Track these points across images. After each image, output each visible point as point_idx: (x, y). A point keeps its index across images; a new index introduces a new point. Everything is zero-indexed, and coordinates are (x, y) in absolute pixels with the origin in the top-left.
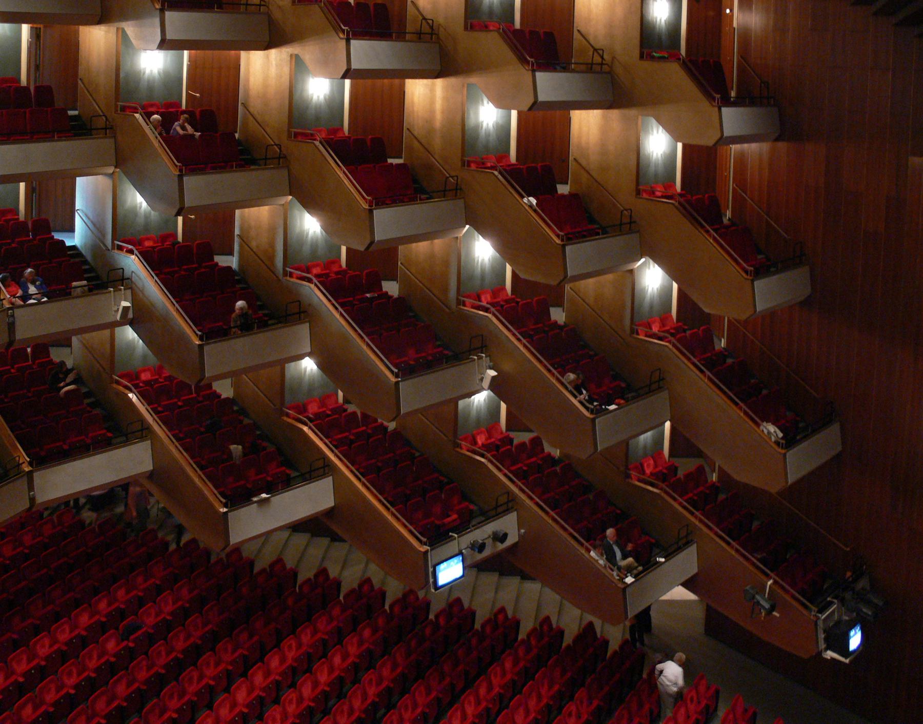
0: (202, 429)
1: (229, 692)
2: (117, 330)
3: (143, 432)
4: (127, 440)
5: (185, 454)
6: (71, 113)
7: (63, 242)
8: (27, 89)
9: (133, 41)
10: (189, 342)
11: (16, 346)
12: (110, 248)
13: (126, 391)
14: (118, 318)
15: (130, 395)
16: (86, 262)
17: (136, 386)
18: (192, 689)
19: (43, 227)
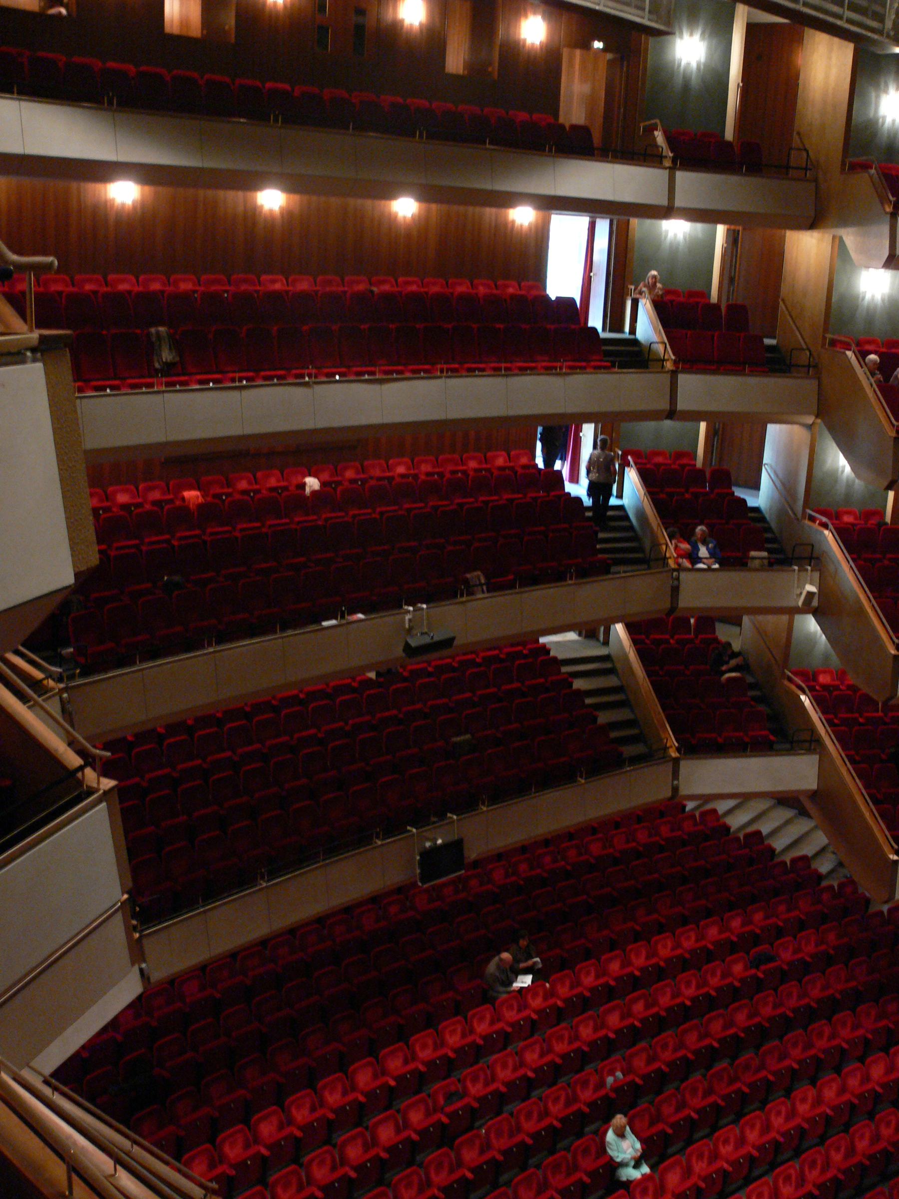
0: (884, 757)
1: (863, 1063)
2: (798, 618)
3: (813, 744)
4: (792, 749)
5: (858, 781)
6: (768, 341)
7: (744, 501)
8: (717, 307)
9: (853, 254)
10: (883, 648)
11: (677, 614)
12: (800, 515)
13: (799, 692)
14: (800, 604)
15: (803, 697)
16: (769, 529)
17: (812, 689)
18: (822, 1043)
19: (723, 479)
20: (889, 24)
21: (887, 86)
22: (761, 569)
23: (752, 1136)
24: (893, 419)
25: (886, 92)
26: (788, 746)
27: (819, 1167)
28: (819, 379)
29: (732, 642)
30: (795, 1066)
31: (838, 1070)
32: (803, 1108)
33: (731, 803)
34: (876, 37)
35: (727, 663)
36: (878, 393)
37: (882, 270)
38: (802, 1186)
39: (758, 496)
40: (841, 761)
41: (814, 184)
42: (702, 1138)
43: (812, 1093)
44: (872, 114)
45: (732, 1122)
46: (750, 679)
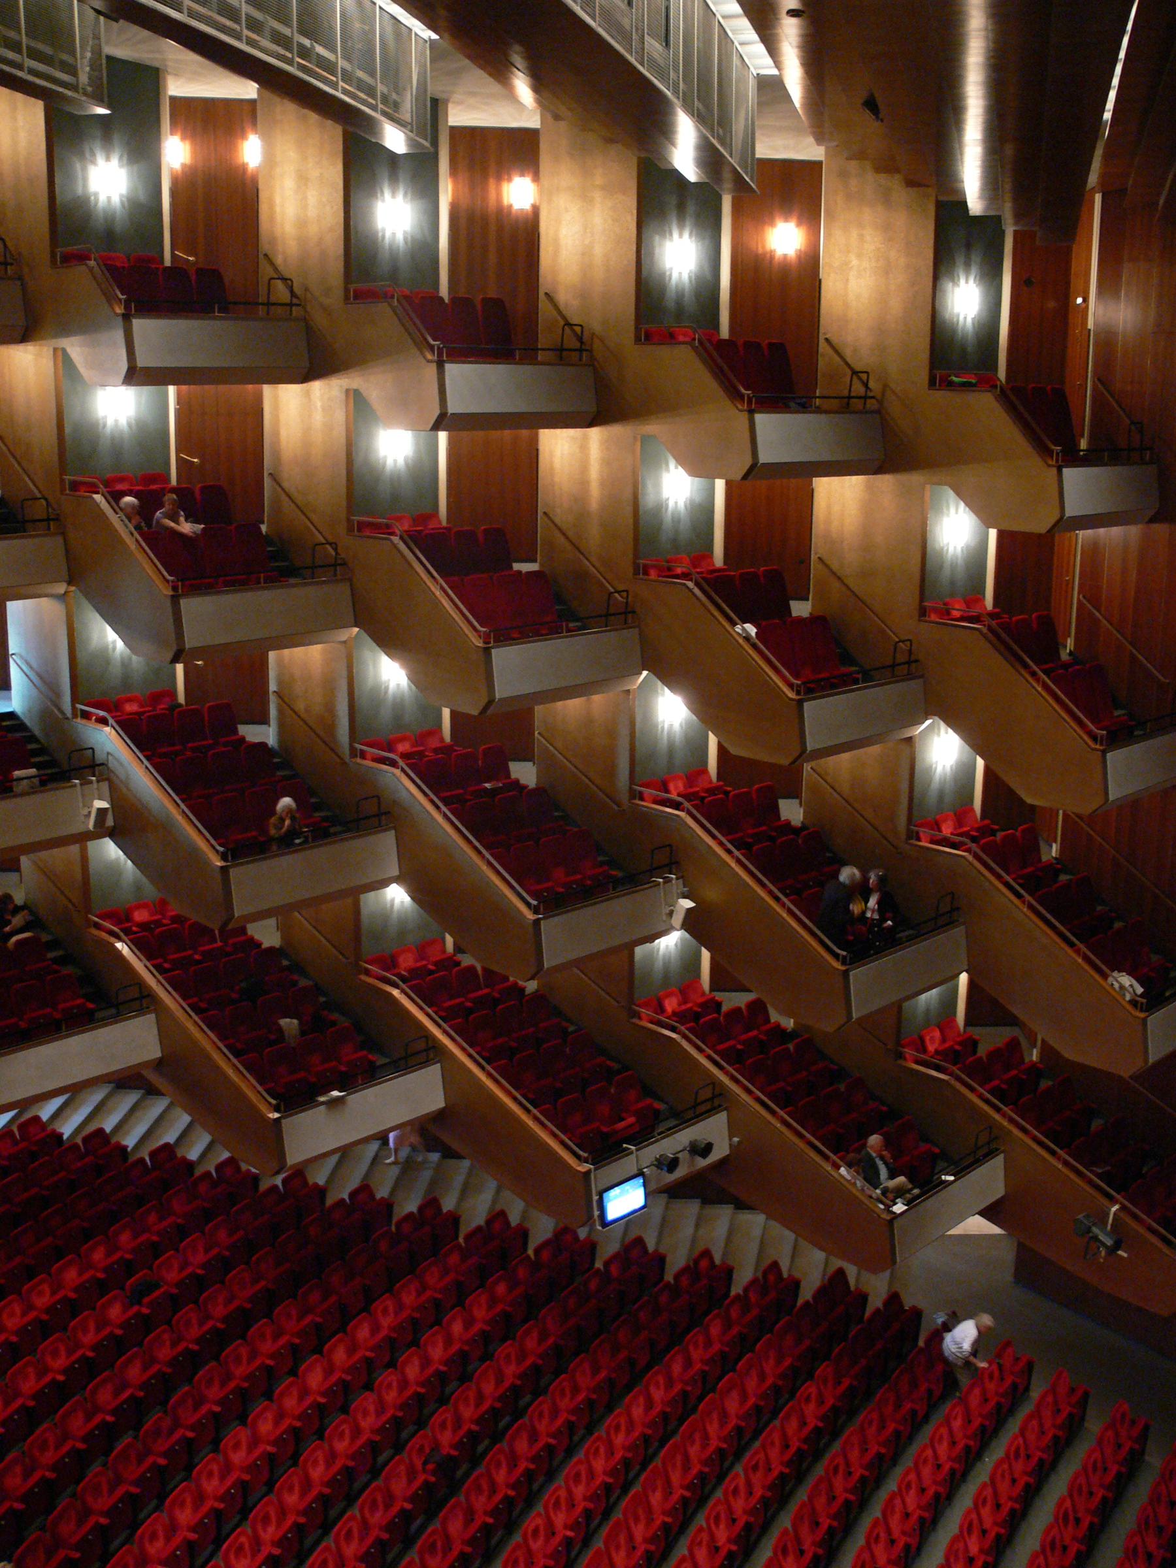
2: (91, 845)
3: (143, 1001)
4: (118, 1014)
5: (209, 1033)
10: (208, 863)
12: (69, 713)
13: (112, 939)
15: (119, 945)
16: (33, 738)
17: (127, 932)
20: (83, 78)
21: (93, 155)
22: (33, 791)
23: (185, 1516)
24: (476, 624)
25: (94, 162)
26: (113, 1011)
27: (274, 1520)
28: (63, 534)
29: (8, 891)
30: (217, 1409)
31: (268, 1395)
32: (238, 1458)
33: (57, 1102)
34: (69, 93)
35: (9, 922)
36: (144, 544)
37: (123, 388)
38: (259, 1551)
39: (10, 699)
40: (181, 1011)
41: (19, 283)
42: (123, 1545)
43: (244, 1435)
44: (80, 191)
45: (156, 1509)
46: (45, 937)
